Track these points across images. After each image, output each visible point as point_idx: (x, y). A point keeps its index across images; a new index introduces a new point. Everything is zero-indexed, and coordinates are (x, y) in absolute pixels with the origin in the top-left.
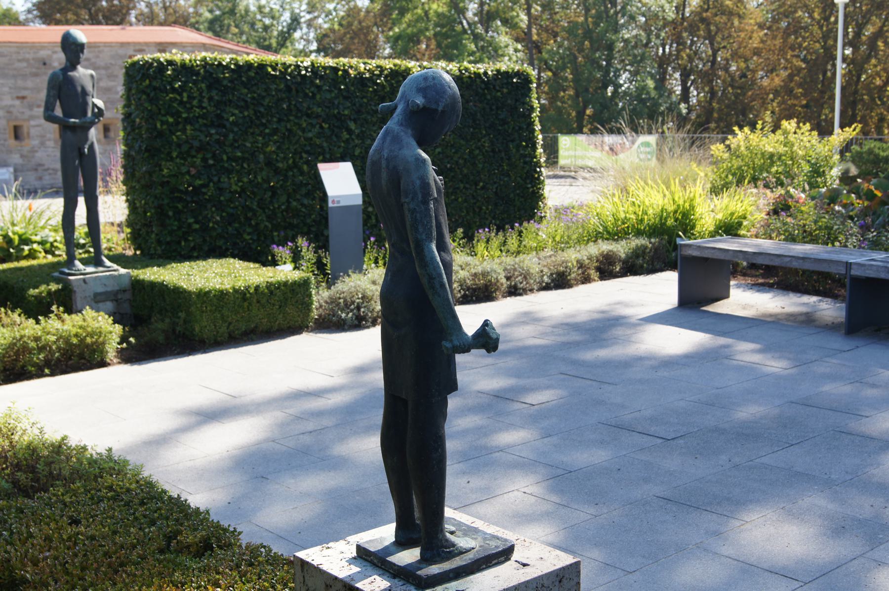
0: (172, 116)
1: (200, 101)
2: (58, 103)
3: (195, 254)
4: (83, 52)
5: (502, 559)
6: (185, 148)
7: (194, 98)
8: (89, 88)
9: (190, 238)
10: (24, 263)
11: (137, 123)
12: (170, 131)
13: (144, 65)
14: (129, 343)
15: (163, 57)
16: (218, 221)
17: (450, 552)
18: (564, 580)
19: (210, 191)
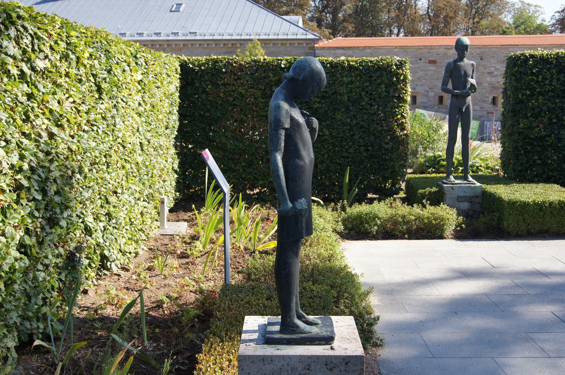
0: (530, 90)
1: (551, 81)
2: (450, 81)
3: (536, 180)
4: (467, 51)
5: (323, 343)
6: (536, 111)
7: (547, 79)
8: (470, 72)
9: (534, 169)
10: (428, 175)
11: (509, 94)
12: (528, 99)
13: (515, 58)
14: (461, 227)
15: (527, 52)
16: (555, 160)
17: (294, 330)
18: (350, 364)
19: (550, 140)
